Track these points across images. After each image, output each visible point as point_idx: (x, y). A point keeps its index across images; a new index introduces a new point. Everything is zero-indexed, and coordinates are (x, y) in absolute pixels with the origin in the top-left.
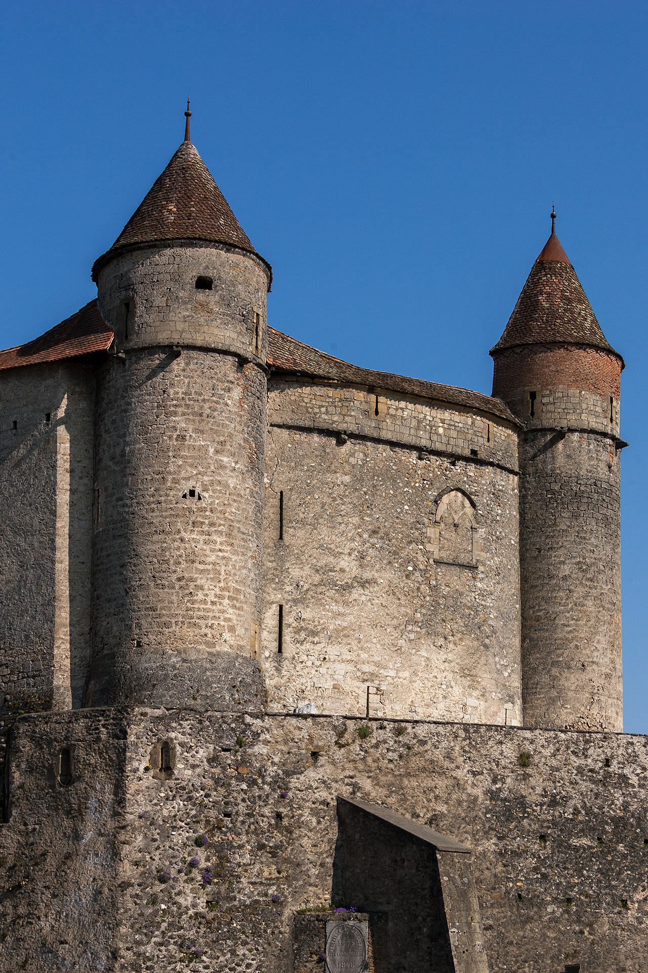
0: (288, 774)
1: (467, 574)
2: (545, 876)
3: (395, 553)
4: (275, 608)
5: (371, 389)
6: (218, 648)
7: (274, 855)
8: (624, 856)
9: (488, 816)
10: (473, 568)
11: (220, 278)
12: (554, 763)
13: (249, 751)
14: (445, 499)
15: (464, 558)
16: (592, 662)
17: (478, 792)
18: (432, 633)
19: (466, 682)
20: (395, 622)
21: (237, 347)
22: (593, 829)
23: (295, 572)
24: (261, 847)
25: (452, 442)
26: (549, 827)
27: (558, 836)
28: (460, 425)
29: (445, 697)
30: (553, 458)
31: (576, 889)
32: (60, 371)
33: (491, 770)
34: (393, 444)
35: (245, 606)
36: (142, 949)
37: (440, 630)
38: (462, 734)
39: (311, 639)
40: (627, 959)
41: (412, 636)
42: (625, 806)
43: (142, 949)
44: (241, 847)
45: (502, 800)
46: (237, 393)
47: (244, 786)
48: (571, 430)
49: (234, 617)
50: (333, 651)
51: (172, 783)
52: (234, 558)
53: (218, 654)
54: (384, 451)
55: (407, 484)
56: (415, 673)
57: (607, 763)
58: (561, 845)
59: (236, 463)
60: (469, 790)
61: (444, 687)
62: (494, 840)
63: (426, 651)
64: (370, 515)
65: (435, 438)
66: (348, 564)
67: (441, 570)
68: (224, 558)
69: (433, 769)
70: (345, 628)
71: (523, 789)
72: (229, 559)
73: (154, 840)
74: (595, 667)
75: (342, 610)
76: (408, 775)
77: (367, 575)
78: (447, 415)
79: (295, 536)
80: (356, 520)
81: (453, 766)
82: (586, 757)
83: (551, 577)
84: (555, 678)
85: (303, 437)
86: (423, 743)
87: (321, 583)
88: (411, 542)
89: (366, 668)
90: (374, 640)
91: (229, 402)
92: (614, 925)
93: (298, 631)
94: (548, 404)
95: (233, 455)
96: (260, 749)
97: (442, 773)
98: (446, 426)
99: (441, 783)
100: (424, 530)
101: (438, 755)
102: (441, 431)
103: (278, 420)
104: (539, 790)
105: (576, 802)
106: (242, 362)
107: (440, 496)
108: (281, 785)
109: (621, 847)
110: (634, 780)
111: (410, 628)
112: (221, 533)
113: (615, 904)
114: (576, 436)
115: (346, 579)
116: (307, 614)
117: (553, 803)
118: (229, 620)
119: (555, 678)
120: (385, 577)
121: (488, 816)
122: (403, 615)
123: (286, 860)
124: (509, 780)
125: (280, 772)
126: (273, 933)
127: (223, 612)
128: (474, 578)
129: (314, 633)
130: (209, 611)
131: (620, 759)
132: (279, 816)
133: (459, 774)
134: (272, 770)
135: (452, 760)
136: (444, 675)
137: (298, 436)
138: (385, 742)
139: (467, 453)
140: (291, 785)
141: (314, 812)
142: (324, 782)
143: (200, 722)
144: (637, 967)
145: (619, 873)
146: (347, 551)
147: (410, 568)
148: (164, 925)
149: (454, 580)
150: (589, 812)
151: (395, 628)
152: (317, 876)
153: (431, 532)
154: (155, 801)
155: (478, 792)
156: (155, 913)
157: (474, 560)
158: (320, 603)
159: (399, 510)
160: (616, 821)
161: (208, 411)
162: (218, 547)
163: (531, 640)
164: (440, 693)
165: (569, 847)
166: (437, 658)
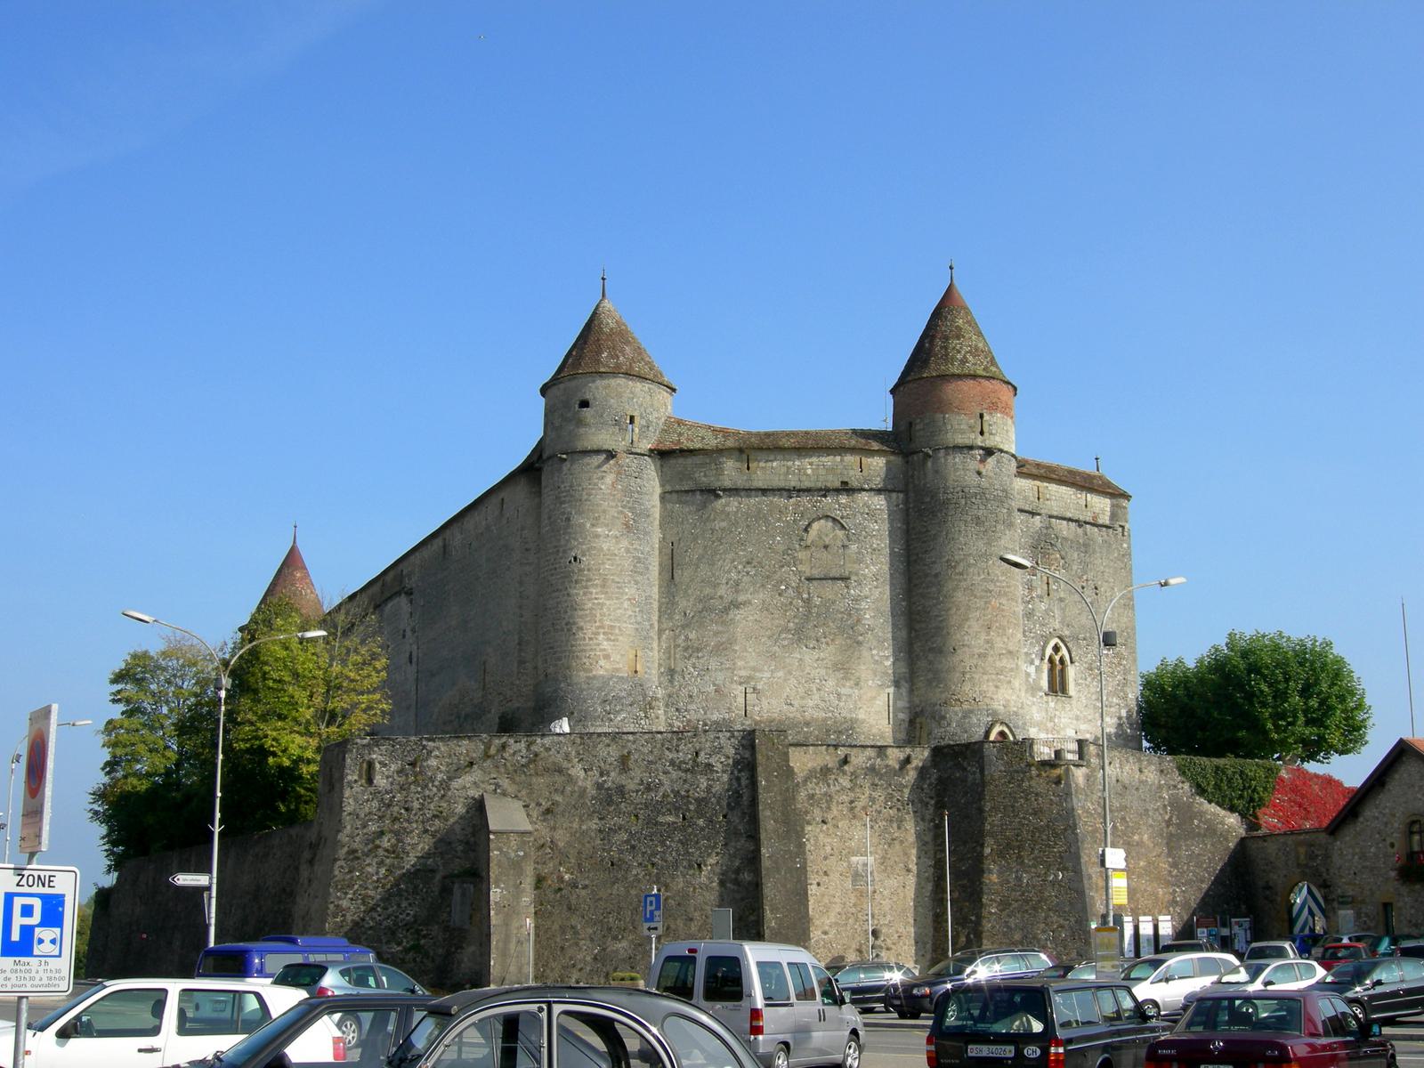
0: (450, 779)
1: (841, 584)
2: (633, 847)
3: (768, 577)
6: (594, 673)
8: (702, 829)
9: (593, 802)
10: (845, 579)
11: (595, 399)
13: (425, 764)
14: (816, 526)
15: (834, 573)
16: (963, 645)
17: (589, 784)
19: (840, 675)
20: (769, 633)
22: (677, 809)
24: (426, 831)
25: (821, 478)
26: (641, 809)
27: (649, 815)
28: (829, 463)
29: (819, 690)
30: (925, 474)
31: (658, 857)
32: (522, 479)
33: (600, 767)
34: (764, 491)
35: (621, 638)
36: (341, 902)
38: (578, 741)
39: (695, 654)
40: (695, 910)
41: (786, 643)
42: (709, 788)
43: (341, 902)
44: (412, 832)
45: (606, 789)
47: (419, 789)
49: (609, 647)
51: (371, 789)
52: (608, 602)
55: (779, 520)
56: (790, 673)
58: (651, 822)
59: (610, 531)
61: (818, 681)
62: (596, 821)
64: (744, 550)
65: (804, 478)
67: (813, 586)
68: (599, 604)
70: (724, 643)
71: (623, 780)
72: (603, 604)
73: (357, 829)
74: (966, 649)
75: (720, 629)
79: (683, 575)
81: (570, 765)
82: (678, 752)
83: (927, 575)
84: (931, 663)
86: (548, 749)
88: (783, 566)
90: (750, 650)
91: (603, 487)
92: (689, 883)
94: (920, 430)
95: (607, 525)
96: (433, 762)
98: (814, 467)
100: (796, 555)
101: (559, 758)
102: (809, 472)
105: (667, 787)
107: (809, 525)
109: (701, 822)
110: (718, 767)
111: (784, 636)
112: (597, 585)
113: (691, 867)
117: (648, 788)
118: (605, 650)
119: (931, 663)
121: (593, 802)
122: (777, 627)
124: (613, 774)
125: (445, 777)
126: (427, 892)
127: (599, 645)
128: (847, 587)
129: (698, 650)
130: (586, 645)
131: (708, 751)
135: (569, 761)
136: (817, 671)
138: (520, 751)
140: (451, 787)
142: (475, 783)
143: (393, 746)
144: (704, 917)
145: (697, 843)
146: (724, 581)
147: (783, 587)
148: (356, 887)
151: (769, 638)
152: (462, 851)
153: (801, 555)
154: (361, 802)
156: (352, 878)
157: (847, 572)
159: (771, 542)
160: (699, 801)
161: (585, 497)
162: (593, 596)
163: (916, 631)
165: (656, 823)
166: (809, 657)
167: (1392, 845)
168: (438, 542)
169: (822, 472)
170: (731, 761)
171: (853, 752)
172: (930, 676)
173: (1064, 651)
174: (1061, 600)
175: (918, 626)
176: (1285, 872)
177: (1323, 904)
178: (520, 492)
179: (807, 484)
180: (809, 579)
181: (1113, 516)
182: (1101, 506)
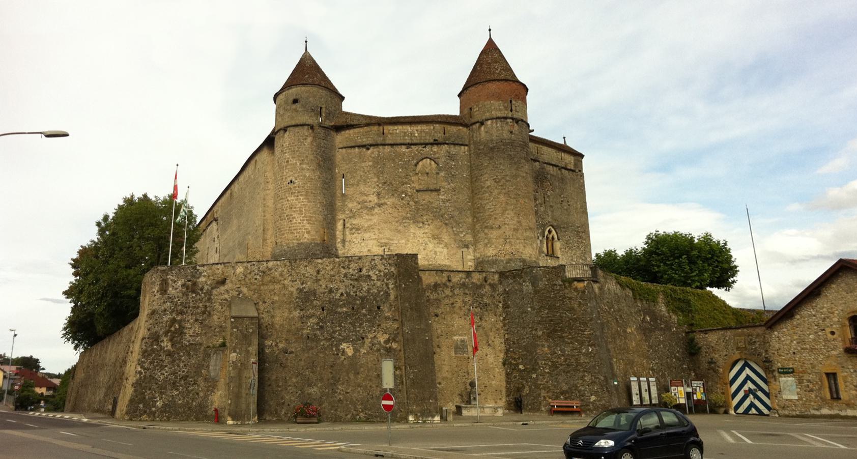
0: (212, 289)
4: (342, 221)
5: (379, 125)
7: (201, 323)
10: (437, 190)
12: (332, 273)
15: (432, 187)
18: (416, 222)
19: (436, 241)
21: (310, 121)
22: (350, 303)
23: (350, 205)
37: (420, 219)
42: (369, 289)
46: (309, 139)
48: (487, 120)
50: (366, 235)
53: (302, 243)
54: (388, 149)
57: (360, 270)
58: (332, 312)
60: (290, 289)
63: (413, 229)
66: (374, 199)
69: (275, 281)
76: (263, 284)
77: (382, 201)
78: (419, 127)
80: (376, 180)
83: (483, 187)
84: (486, 234)
85: (352, 150)
86: (270, 270)
87: (361, 208)
89: (383, 241)
93: (351, 229)
96: (202, 279)
97: (278, 282)
99: (277, 287)
103: (341, 146)
104: (324, 286)
106: (312, 128)
108: (209, 293)
109: (364, 311)
110: (374, 277)
114: (489, 122)
115: (372, 204)
116: (355, 222)
120: (390, 201)
123: (206, 325)
129: (358, 229)
132: (206, 307)
133: (286, 282)
134: (206, 287)
137: (349, 150)
139: (432, 141)
141: (221, 304)
145: (361, 324)
149: (427, 197)
150: (348, 294)
155: (293, 289)
158: (360, 216)
160: (362, 298)
164: (422, 248)
165: (336, 313)
166: (419, 233)
167: (833, 333)
168: (229, 192)
169: (424, 135)
170: (382, 274)
171: (452, 274)
172: (486, 241)
173: (554, 231)
174: (551, 206)
175: (478, 215)
176: (725, 353)
177: (764, 375)
178: (265, 153)
179: (415, 141)
180: (418, 191)
181: (575, 165)
182: (569, 159)
